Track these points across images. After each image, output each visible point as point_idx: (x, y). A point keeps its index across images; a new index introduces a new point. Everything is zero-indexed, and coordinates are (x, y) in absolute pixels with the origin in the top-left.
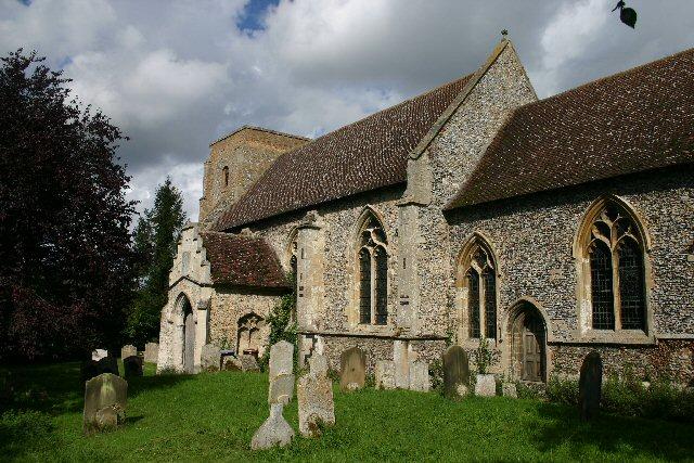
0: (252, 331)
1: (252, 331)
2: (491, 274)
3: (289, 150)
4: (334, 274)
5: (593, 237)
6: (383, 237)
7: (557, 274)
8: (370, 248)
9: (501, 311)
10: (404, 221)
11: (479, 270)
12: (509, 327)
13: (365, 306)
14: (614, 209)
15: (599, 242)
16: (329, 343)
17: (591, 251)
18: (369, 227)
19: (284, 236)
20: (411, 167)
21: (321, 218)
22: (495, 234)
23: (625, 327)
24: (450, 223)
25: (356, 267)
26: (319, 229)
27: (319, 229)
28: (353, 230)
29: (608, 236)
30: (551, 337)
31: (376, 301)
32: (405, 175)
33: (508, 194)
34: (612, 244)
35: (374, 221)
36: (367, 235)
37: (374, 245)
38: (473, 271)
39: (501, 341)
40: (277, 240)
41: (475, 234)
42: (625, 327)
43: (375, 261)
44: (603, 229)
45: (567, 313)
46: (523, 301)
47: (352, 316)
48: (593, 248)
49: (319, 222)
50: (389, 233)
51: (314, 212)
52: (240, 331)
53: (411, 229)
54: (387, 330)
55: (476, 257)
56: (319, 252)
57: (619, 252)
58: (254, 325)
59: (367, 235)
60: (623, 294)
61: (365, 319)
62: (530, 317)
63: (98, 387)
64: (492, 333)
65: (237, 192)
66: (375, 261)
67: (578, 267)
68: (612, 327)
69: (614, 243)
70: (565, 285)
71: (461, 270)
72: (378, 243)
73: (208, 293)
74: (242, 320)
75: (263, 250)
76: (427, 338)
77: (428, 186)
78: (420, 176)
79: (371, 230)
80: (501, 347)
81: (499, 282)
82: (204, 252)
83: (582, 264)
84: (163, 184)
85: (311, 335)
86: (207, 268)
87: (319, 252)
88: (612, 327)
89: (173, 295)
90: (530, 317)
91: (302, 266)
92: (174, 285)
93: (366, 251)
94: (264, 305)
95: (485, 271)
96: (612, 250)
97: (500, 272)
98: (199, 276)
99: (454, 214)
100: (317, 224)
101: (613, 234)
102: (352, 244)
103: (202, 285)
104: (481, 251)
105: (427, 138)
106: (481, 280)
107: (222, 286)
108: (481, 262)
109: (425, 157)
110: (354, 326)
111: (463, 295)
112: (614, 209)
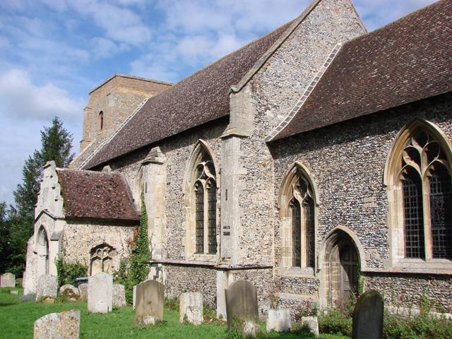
0: (105, 259)
1: (105, 259)
2: (310, 203)
3: (156, 94)
4: (174, 205)
5: (404, 163)
6: (213, 172)
7: (371, 202)
8: (203, 182)
9: (318, 237)
10: (227, 154)
11: (300, 200)
12: (327, 257)
13: (200, 236)
14: (424, 135)
15: (410, 169)
16: (171, 271)
17: (402, 178)
18: (203, 160)
19: (135, 173)
20: (235, 101)
21: (162, 155)
22: (312, 164)
23: (436, 255)
24: (275, 155)
25: (191, 198)
26: (162, 164)
27: (162, 164)
28: (188, 164)
29: (418, 162)
30: (364, 267)
31: (210, 232)
32: (228, 108)
33: (327, 122)
34: (423, 170)
35: (206, 156)
36: (200, 168)
37: (206, 177)
38: (295, 203)
39: (319, 270)
40: (129, 175)
41: (296, 164)
42: (436, 255)
43: (208, 189)
44: (414, 155)
45: (381, 243)
46: (338, 231)
47: (188, 246)
48: (404, 175)
49: (161, 158)
50: (217, 170)
51: (158, 149)
52: (93, 260)
53: (238, 158)
54: (214, 260)
55: (298, 187)
56: (158, 184)
57: (429, 178)
58: (106, 255)
59: (200, 168)
60: (434, 222)
61: (200, 249)
62: (345, 247)
63: (149, 271)
64: (312, 263)
65: (110, 134)
66: (208, 189)
67: (390, 195)
68: (423, 256)
69: (425, 168)
70: (379, 212)
71: (285, 202)
72: (210, 175)
73: (61, 226)
74: (93, 251)
75: (117, 184)
76: (250, 267)
77: (251, 118)
78: (243, 109)
79: (204, 163)
80: (319, 276)
81: (317, 210)
82: (59, 188)
83: (395, 193)
84: (51, 125)
85: (155, 263)
86: (61, 202)
87: (158, 184)
88: (423, 256)
89: (37, 227)
90: (345, 247)
91: (149, 199)
92: (38, 218)
93: (199, 183)
94: (118, 237)
95: (305, 200)
96: (422, 177)
97: (318, 201)
98: (54, 211)
99: (278, 147)
100: (159, 159)
101: (424, 159)
102: (188, 177)
103: (55, 219)
104: (304, 184)
105: (252, 71)
106: (303, 204)
107: (70, 219)
108: (303, 192)
109: (248, 90)
110: (190, 255)
111: (287, 224)
112: (424, 135)
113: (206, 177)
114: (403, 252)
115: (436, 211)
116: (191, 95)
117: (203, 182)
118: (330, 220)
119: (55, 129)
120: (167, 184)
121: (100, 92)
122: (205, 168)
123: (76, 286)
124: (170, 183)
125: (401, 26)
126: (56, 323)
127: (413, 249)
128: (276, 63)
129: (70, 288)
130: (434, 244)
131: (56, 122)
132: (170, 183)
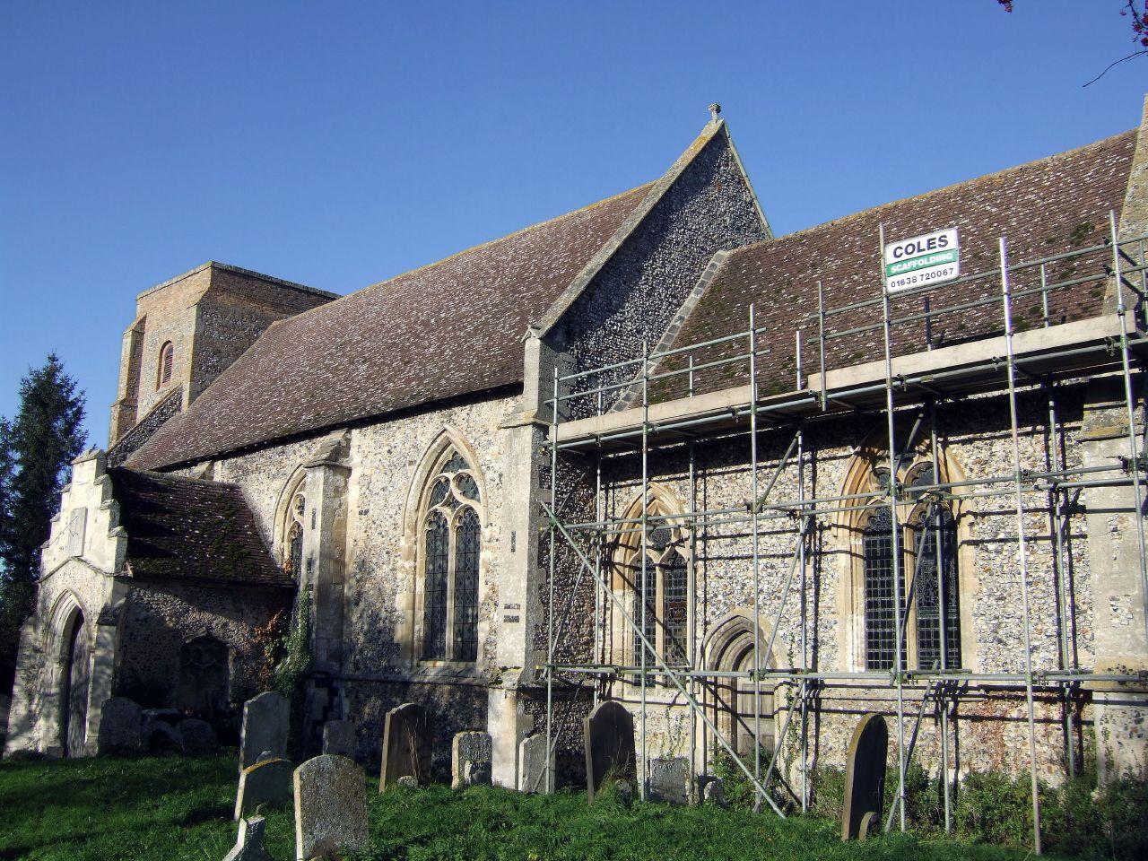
8: (447, 512)
72: (464, 501)
113: (452, 503)
114: (862, 660)
115: (928, 585)
116: (398, 326)
117: (447, 512)
118: (720, 597)
119: (52, 372)
120: (360, 513)
121: (166, 298)
122: (452, 485)
123: (173, 725)
124: (366, 512)
125: (849, 235)
126: (331, 773)
127: (876, 595)
128: (610, 285)
129: (164, 729)
130: (922, 645)
131: (53, 359)
132: (366, 512)
